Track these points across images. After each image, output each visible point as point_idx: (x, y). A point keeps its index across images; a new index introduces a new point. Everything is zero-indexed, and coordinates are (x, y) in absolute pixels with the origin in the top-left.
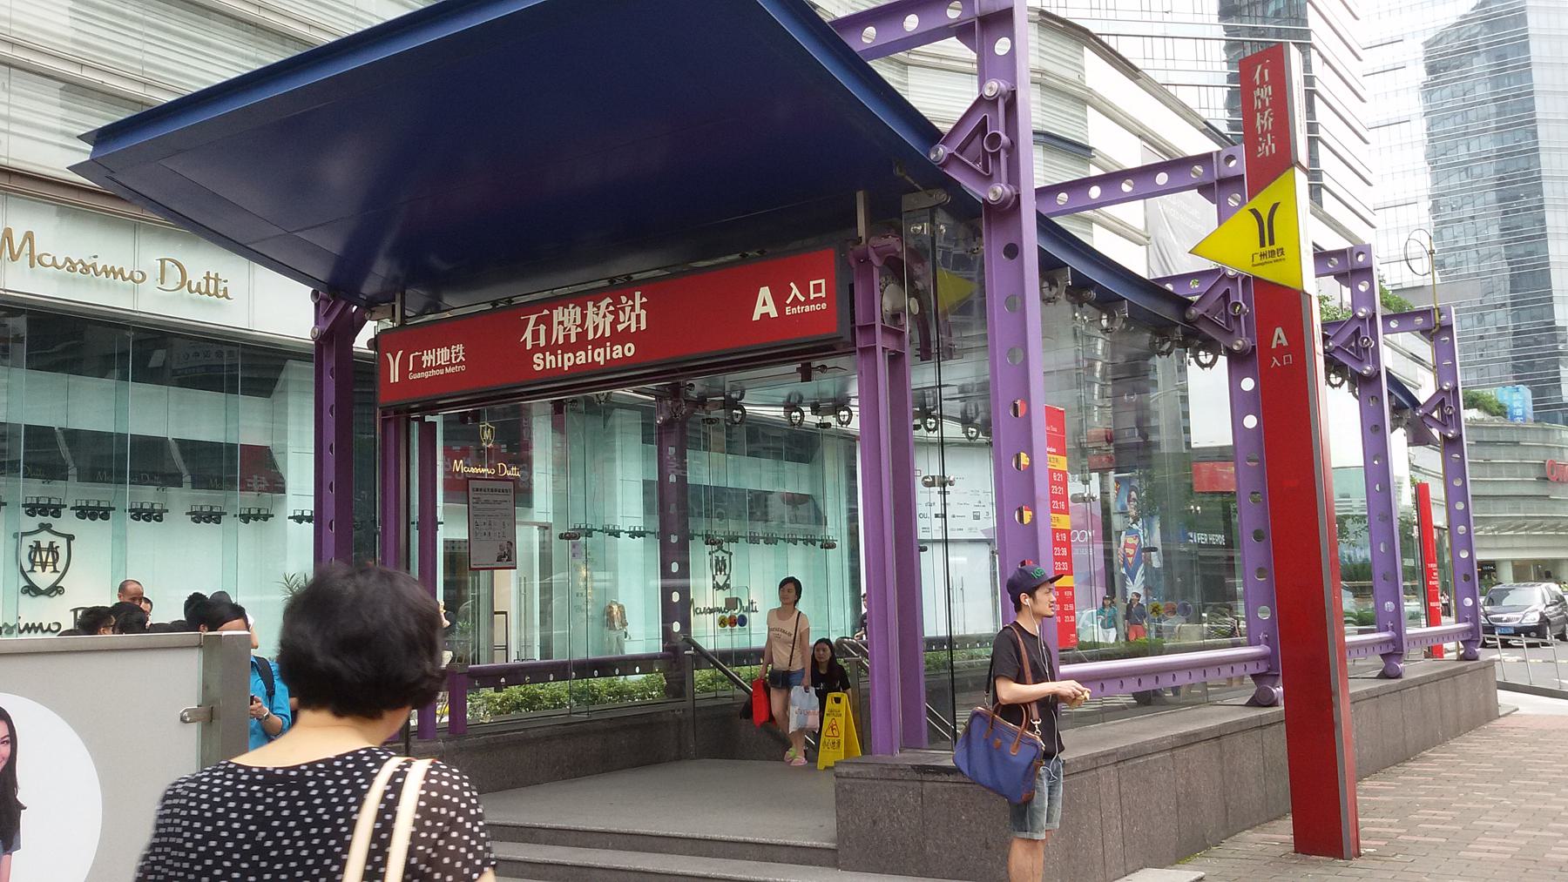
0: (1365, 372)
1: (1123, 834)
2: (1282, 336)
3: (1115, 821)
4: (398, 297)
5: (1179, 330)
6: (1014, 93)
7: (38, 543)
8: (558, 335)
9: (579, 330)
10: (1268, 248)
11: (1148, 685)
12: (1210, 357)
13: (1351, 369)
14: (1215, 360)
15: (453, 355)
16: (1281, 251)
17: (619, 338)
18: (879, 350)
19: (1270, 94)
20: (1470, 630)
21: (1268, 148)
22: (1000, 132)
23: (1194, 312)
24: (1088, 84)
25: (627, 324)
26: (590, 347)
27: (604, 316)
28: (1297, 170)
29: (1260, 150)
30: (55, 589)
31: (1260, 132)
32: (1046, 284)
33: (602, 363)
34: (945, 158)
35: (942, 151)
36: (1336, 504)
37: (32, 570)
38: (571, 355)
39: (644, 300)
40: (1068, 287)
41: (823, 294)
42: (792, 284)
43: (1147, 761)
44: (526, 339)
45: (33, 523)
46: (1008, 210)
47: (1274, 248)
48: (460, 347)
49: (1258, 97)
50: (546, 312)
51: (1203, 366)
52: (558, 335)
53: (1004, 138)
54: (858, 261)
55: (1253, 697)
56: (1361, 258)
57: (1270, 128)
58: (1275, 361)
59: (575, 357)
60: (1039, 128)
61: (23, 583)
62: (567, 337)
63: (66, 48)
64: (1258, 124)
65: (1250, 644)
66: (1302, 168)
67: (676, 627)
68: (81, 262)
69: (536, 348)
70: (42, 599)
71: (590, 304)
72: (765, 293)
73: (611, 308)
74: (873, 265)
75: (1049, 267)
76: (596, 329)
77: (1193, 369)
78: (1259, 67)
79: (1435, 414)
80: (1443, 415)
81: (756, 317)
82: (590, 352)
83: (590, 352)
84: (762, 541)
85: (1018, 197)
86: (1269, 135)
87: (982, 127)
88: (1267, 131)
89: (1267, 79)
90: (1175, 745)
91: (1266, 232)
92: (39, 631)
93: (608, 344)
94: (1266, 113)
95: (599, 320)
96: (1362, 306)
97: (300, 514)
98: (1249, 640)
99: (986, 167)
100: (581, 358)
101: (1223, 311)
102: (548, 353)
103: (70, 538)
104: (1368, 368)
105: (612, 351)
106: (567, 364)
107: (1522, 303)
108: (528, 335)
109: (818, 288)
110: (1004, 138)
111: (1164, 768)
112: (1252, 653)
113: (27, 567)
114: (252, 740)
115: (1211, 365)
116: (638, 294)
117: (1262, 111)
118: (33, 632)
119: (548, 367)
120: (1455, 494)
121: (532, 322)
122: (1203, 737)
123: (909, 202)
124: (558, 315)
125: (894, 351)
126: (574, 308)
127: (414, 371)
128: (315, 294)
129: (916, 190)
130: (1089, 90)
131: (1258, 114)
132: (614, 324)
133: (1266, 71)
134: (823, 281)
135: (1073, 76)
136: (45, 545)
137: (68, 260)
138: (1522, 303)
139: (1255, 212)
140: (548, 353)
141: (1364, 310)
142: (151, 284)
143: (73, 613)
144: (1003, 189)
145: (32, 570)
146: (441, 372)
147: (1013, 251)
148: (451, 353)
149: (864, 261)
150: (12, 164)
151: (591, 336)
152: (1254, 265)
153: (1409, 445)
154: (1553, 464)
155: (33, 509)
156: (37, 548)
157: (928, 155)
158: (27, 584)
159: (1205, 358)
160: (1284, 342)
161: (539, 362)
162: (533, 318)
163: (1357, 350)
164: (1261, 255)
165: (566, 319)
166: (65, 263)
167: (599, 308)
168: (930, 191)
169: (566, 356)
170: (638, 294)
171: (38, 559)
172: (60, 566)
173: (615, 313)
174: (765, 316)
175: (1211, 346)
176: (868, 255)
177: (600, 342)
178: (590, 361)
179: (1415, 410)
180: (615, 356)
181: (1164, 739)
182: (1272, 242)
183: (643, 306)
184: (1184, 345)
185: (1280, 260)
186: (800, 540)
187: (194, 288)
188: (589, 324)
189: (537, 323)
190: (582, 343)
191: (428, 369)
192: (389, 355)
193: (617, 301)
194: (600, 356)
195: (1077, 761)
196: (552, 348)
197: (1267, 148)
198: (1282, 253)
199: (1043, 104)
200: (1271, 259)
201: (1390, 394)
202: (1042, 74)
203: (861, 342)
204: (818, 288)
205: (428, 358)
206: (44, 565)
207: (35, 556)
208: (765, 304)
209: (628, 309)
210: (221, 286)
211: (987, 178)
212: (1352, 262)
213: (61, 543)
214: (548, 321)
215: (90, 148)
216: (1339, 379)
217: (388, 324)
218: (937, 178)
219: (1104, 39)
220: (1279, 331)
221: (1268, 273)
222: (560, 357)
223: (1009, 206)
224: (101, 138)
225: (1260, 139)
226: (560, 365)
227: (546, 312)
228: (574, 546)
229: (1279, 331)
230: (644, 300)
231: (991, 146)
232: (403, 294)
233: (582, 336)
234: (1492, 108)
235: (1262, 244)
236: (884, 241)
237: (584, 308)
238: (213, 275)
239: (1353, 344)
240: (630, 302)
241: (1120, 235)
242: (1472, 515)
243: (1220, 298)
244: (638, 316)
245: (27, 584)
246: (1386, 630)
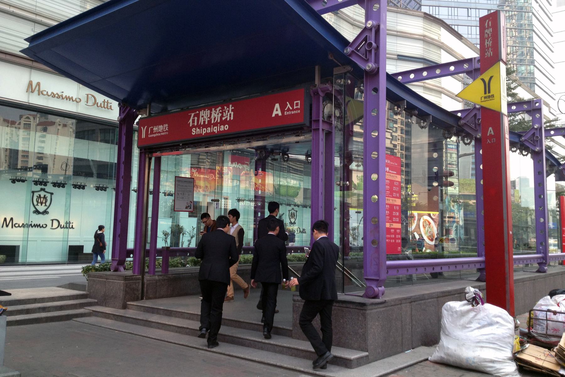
0: (536, 150)
1: (412, 331)
2: (492, 130)
3: (408, 326)
4: (148, 106)
5: (455, 128)
7: (40, 195)
8: (201, 121)
9: (209, 119)
10: (487, 94)
11: (437, 270)
13: (531, 149)
15: (164, 128)
16: (493, 96)
17: (223, 123)
18: (321, 130)
19: (491, 31)
20: (543, 258)
21: (490, 53)
22: (372, 42)
23: (462, 122)
24: (442, 41)
25: (226, 117)
26: (212, 126)
27: (218, 114)
29: (486, 54)
30: (45, 212)
31: (486, 47)
33: (216, 132)
34: (349, 53)
35: (349, 50)
37: (37, 205)
38: (205, 129)
39: (233, 108)
40: (405, 108)
41: (299, 107)
42: (288, 103)
43: (425, 302)
44: (190, 123)
45: (39, 187)
46: (375, 73)
47: (490, 94)
48: (167, 125)
49: (487, 33)
50: (198, 112)
51: (466, 144)
52: (201, 121)
53: (374, 44)
54: (314, 94)
55: (479, 277)
56: (537, 104)
57: (491, 45)
58: (489, 141)
59: (207, 130)
61: (34, 209)
62: (204, 122)
64: (486, 44)
65: (537, 253)
68: (57, 94)
69: (194, 126)
70: (41, 215)
71: (213, 109)
72: (277, 106)
73: (221, 111)
74: (320, 95)
76: (215, 119)
78: (487, 21)
81: (273, 115)
82: (212, 128)
83: (212, 128)
84: (308, 207)
85: (378, 68)
86: (490, 48)
87: (365, 39)
88: (489, 47)
89: (490, 25)
90: (439, 296)
91: (487, 87)
92: (39, 227)
93: (219, 125)
94: (489, 39)
95: (216, 115)
96: (537, 124)
97: (42, 180)
98: (537, 252)
99: (366, 57)
100: (209, 130)
101: (474, 122)
102: (197, 128)
103: (52, 194)
104: (538, 148)
105: (220, 128)
106: (204, 132)
108: (191, 121)
109: (297, 104)
110: (374, 44)
111: (433, 305)
112: (478, 260)
113: (35, 203)
116: (231, 106)
118: (36, 227)
119: (197, 133)
121: (192, 116)
122: (452, 293)
123: (336, 71)
124: (202, 113)
125: (328, 131)
126: (207, 111)
127: (151, 134)
128: (119, 104)
129: (340, 66)
130: (442, 43)
131: (486, 40)
132: (222, 116)
133: (490, 22)
134: (299, 102)
136: (42, 196)
137: (52, 93)
139: (483, 80)
140: (197, 128)
141: (537, 125)
142: (83, 102)
143: (51, 221)
144: (372, 65)
145: (37, 205)
146: (160, 135)
148: (163, 127)
149: (316, 94)
151: (213, 122)
152: (481, 102)
153: (556, 180)
155: (36, 183)
156: (40, 197)
157: (343, 51)
158: (35, 210)
160: (492, 133)
161: (194, 132)
162: (193, 114)
163: (534, 141)
164: (485, 98)
165: (204, 115)
166: (51, 94)
167: (216, 111)
168: (344, 66)
169: (204, 129)
170: (231, 106)
171: (40, 201)
172: (48, 204)
173: (222, 113)
174: (277, 115)
176: (318, 91)
177: (216, 124)
178: (212, 131)
179: (559, 167)
180: (221, 130)
181: (434, 293)
182: (489, 92)
183: (232, 110)
185: (493, 99)
186: (293, 205)
187: (99, 105)
188: (213, 117)
189: (194, 117)
190: (210, 124)
191: (155, 133)
192: (142, 128)
193: (223, 108)
194: (215, 130)
195: (393, 300)
196: (199, 126)
197: (489, 54)
198: (493, 97)
199: (424, 48)
200: (489, 99)
201: (547, 160)
202: (424, 36)
203: (314, 127)
204: (297, 104)
205: (155, 129)
206: (42, 203)
207: (38, 200)
208: (277, 110)
209: (227, 112)
210: (109, 105)
211: (367, 61)
212: (533, 106)
213: (48, 196)
214: (198, 116)
215: (29, 44)
216: (526, 153)
217: (145, 116)
218: (346, 61)
219: (453, 27)
220: (490, 129)
221: (488, 104)
222: (201, 129)
223: (375, 72)
224: (31, 39)
225: (487, 50)
226: (201, 133)
227: (198, 112)
228: (217, 204)
229: (490, 129)
230: (233, 108)
232: (150, 105)
233: (210, 122)
235: (485, 93)
236: (325, 86)
237: (211, 111)
238: (106, 101)
239: (532, 139)
240: (228, 109)
241: (452, 98)
243: (473, 117)
244: (230, 114)
245: (35, 210)
246: (540, 253)
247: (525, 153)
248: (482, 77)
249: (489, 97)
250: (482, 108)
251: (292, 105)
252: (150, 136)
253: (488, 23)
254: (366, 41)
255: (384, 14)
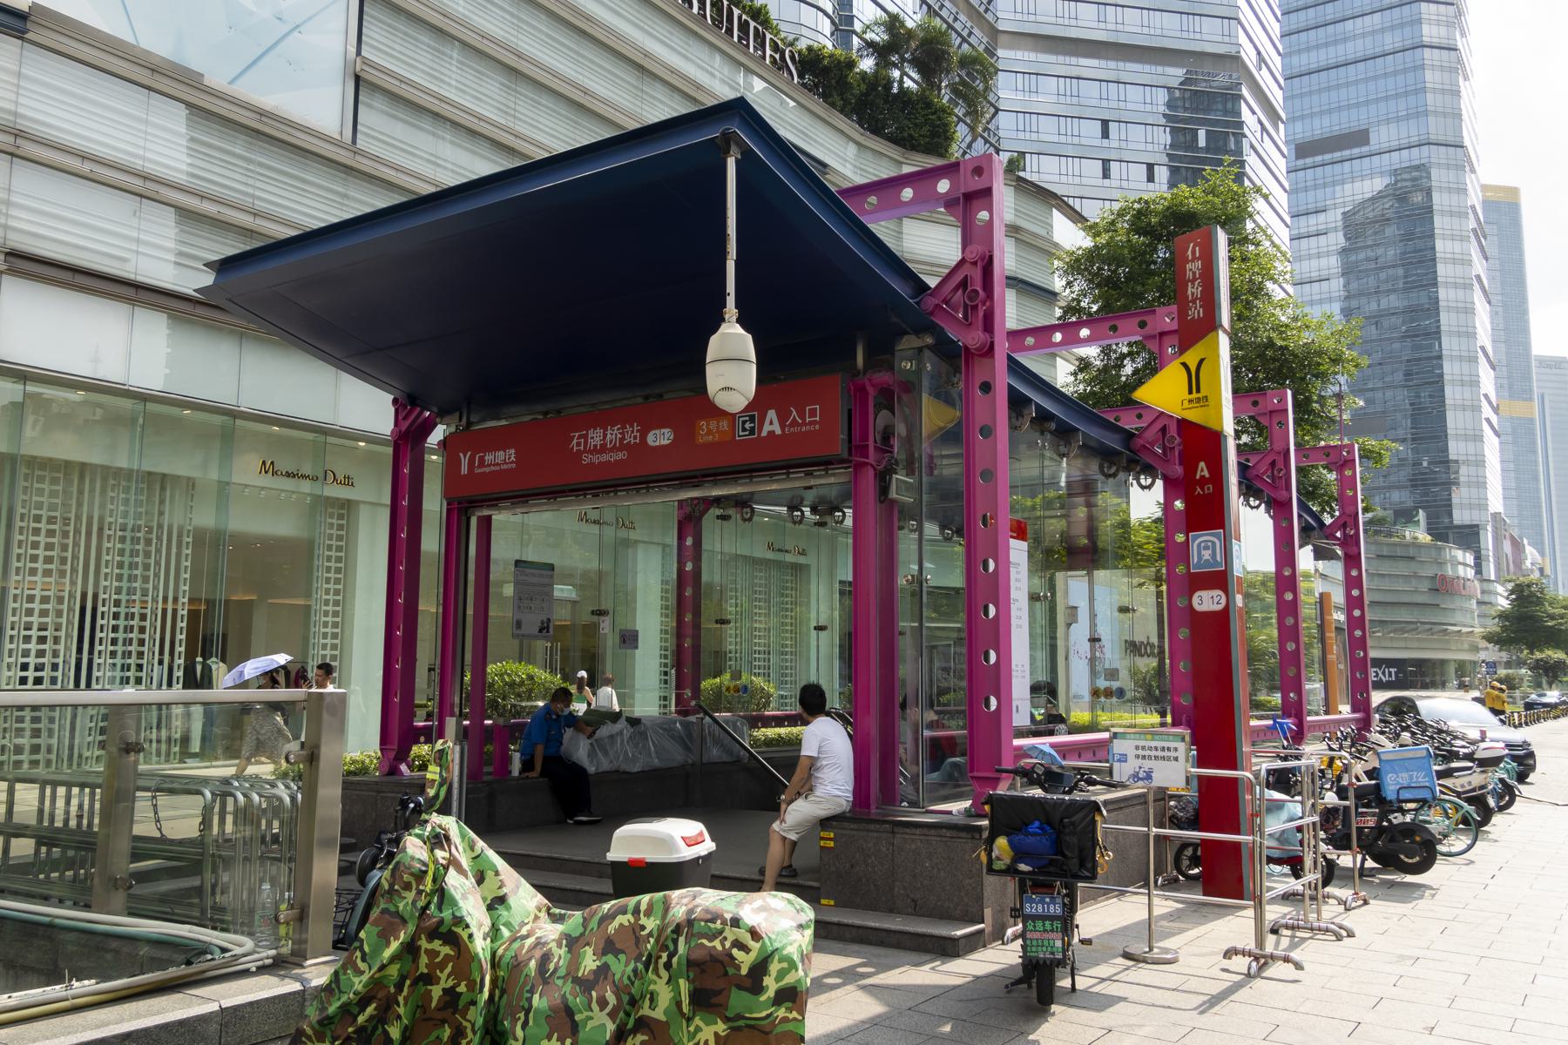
6: (991, 258)
10: (1195, 395)
12: (1149, 481)
14: (1153, 484)
21: (1196, 312)
28: (1220, 333)
32: (1014, 415)
36: (46, 824)
47: (1200, 395)
51: (1143, 487)
60: (1013, 274)
63: (181, 178)
66: (1225, 331)
67: (688, 693)
75: (1017, 402)
77: (1135, 490)
79: (1338, 534)
80: (1344, 534)
85: (992, 344)
87: (964, 284)
91: (1194, 381)
107: (1421, 439)
109: (813, 413)
114: (648, 724)
115: (1149, 487)
117: (1193, 281)
120: (1353, 603)
127: (479, 466)
128: (395, 402)
135: (1042, 232)
138: (1421, 439)
139: (1184, 365)
146: (497, 468)
147: (987, 387)
150: (140, 279)
154: (1443, 577)
159: (1146, 481)
160: (1206, 474)
174: (771, 433)
175: (1149, 470)
182: (1198, 391)
184: (1128, 470)
191: (489, 465)
201: (1300, 516)
204: (813, 413)
205: (489, 458)
208: (771, 423)
219: (1071, 201)
220: (1202, 464)
221: (1193, 416)
224: (224, 266)
229: (1202, 464)
231: (971, 299)
234: (1400, 271)
235: (1190, 392)
242: (1367, 618)
247: (1252, 502)
248: (1182, 359)
249: (1198, 400)
250: (1183, 424)
251: (802, 415)
252: (477, 471)
253: (1194, 248)
254: (965, 288)
255: (587, 459)
